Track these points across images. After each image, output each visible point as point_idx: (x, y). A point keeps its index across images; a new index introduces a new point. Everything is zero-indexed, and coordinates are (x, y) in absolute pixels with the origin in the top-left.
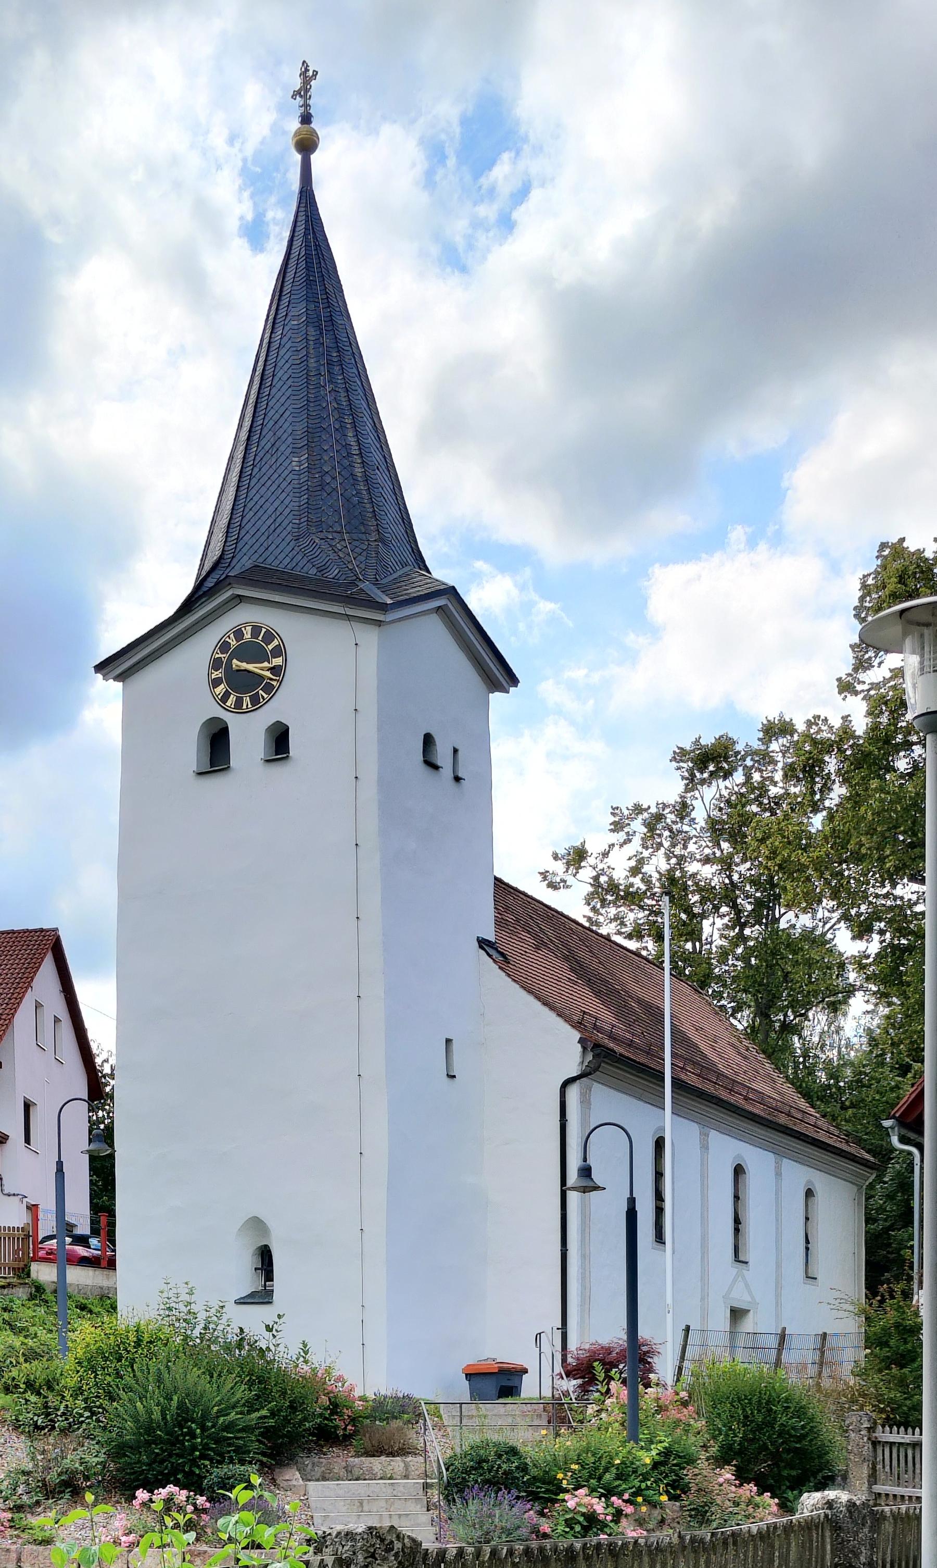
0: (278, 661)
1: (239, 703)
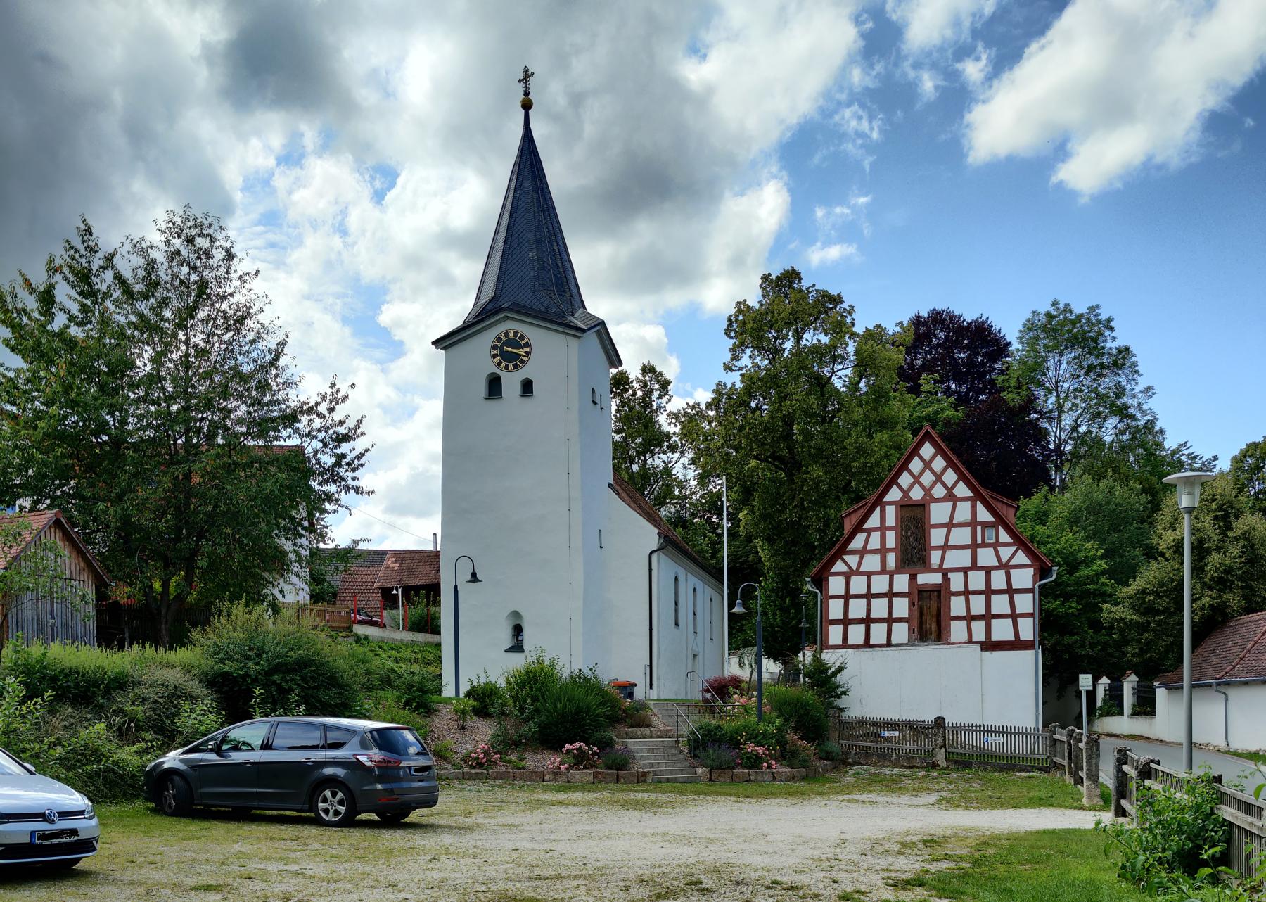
0: (527, 349)
1: (507, 367)
